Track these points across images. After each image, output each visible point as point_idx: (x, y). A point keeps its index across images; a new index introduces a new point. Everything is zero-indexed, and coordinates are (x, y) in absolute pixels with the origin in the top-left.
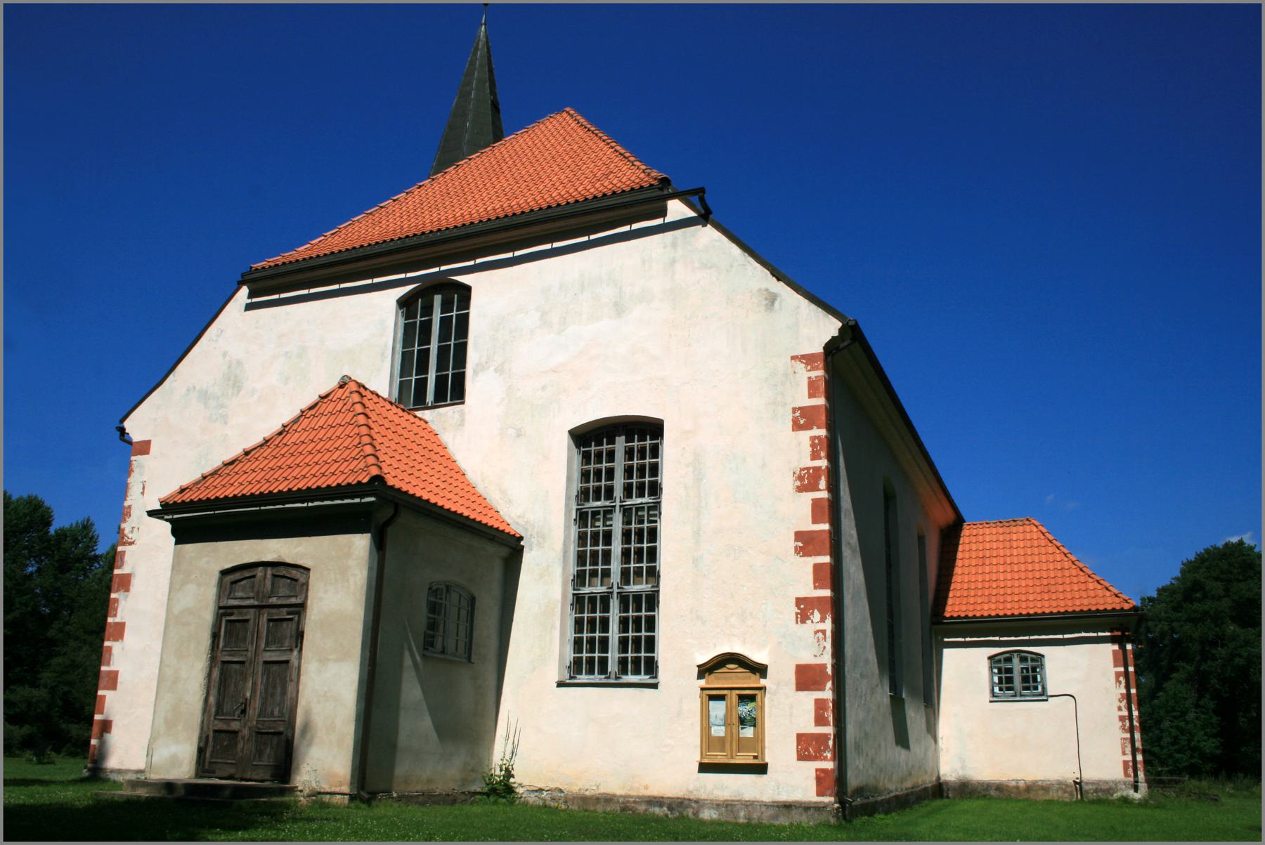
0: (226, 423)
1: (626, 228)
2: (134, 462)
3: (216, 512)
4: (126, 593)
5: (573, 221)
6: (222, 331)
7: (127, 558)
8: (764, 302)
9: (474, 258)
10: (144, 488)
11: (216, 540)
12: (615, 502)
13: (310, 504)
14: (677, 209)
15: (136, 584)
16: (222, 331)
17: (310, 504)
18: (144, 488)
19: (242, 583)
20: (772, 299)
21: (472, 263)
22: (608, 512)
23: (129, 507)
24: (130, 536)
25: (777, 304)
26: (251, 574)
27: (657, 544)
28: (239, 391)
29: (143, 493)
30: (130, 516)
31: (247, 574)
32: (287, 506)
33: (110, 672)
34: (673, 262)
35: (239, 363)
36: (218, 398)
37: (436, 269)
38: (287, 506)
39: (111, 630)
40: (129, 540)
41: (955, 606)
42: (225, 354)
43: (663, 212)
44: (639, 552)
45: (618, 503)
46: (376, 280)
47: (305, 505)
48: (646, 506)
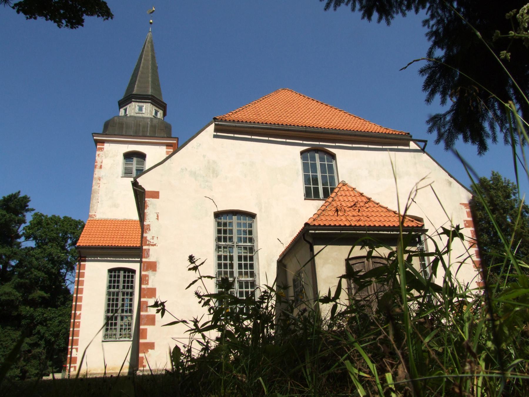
0: (212, 190)
1: (396, 147)
2: (147, 202)
3: (316, 232)
4: (154, 272)
5: (377, 139)
6: (200, 144)
7: (151, 252)
8: (448, 184)
9: (335, 143)
10: (158, 216)
11: (340, 245)
12: (234, 243)
13: (392, 233)
14: (413, 145)
15: (160, 267)
16: (200, 144)
17: (392, 233)
18: (158, 216)
19: (357, 265)
20: (450, 183)
21: (334, 144)
22: (232, 247)
23: (149, 225)
24: (152, 241)
25: (452, 185)
26: (362, 261)
27: (217, 262)
28: (217, 176)
29: (158, 219)
30: (150, 230)
31: (359, 261)
32: (380, 232)
33: (148, 316)
34: (415, 164)
35: (214, 162)
36: (204, 177)
37: (318, 143)
38: (380, 232)
39: (145, 292)
40: (152, 243)
41: (271, 287)
42: (204, 156)
43: (408, 145)
44: (246, 265)
45: (235, 245)
46: (384, 147)
47: (389, 233)
48: (222, 246)
